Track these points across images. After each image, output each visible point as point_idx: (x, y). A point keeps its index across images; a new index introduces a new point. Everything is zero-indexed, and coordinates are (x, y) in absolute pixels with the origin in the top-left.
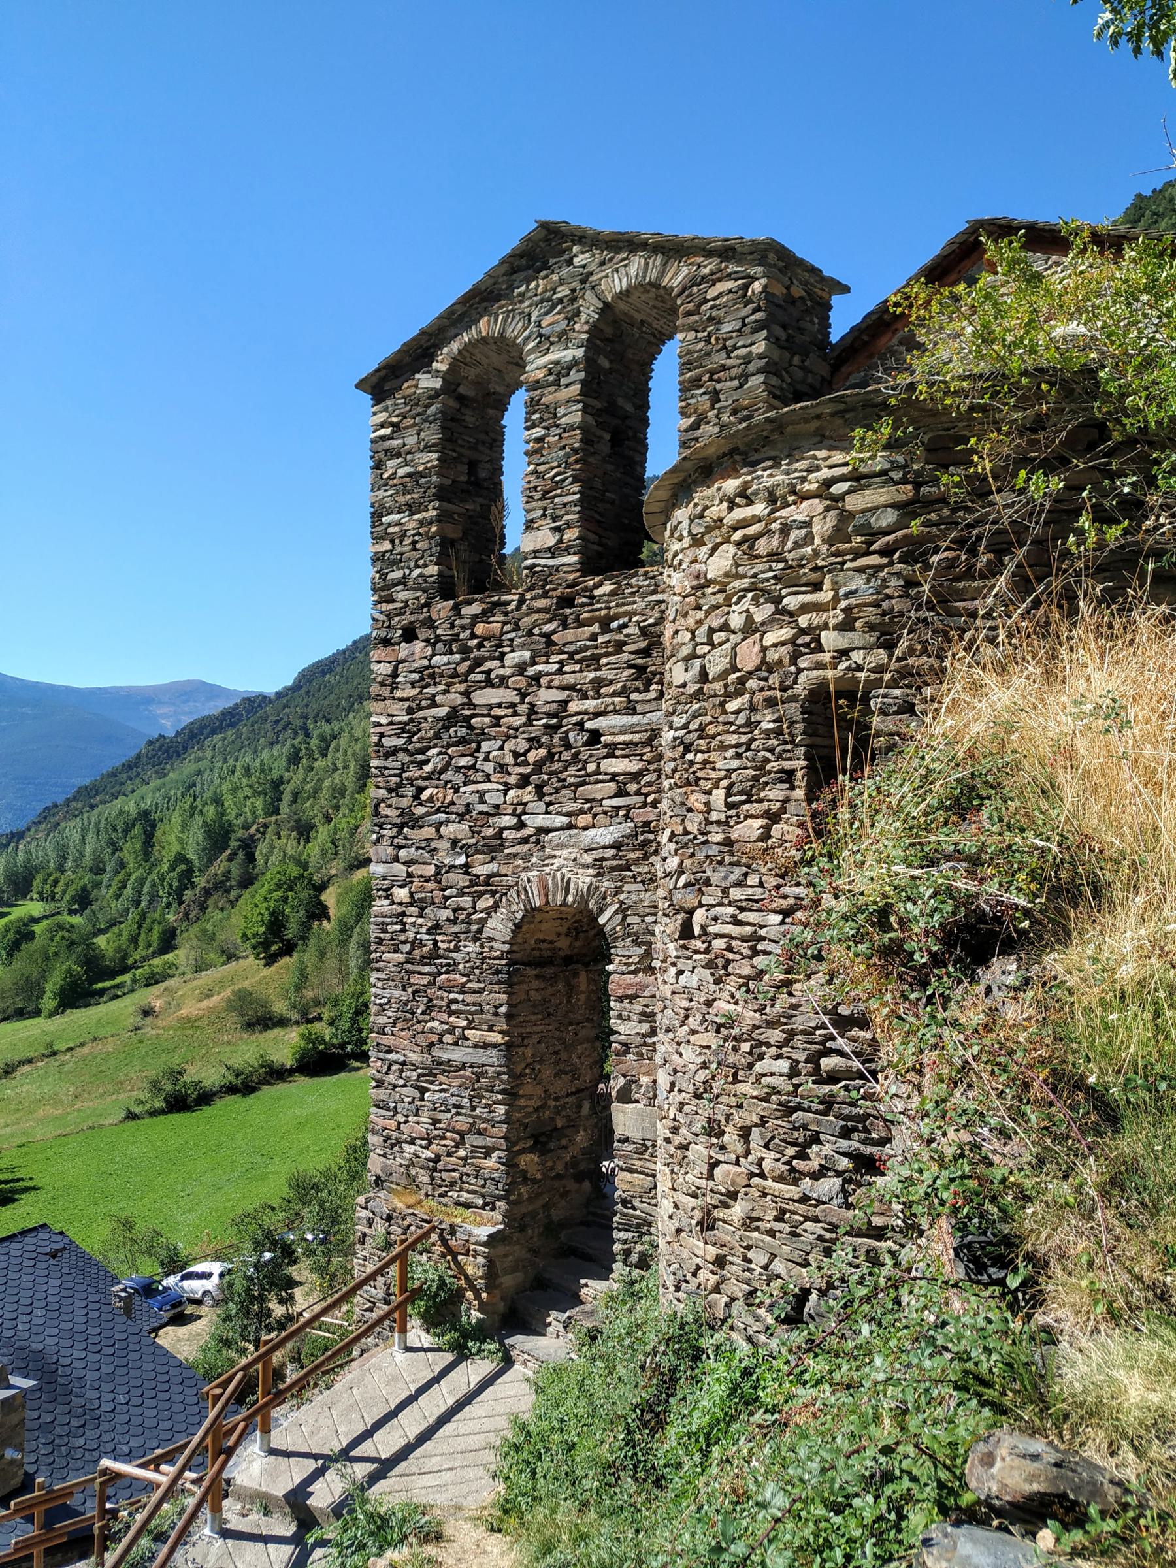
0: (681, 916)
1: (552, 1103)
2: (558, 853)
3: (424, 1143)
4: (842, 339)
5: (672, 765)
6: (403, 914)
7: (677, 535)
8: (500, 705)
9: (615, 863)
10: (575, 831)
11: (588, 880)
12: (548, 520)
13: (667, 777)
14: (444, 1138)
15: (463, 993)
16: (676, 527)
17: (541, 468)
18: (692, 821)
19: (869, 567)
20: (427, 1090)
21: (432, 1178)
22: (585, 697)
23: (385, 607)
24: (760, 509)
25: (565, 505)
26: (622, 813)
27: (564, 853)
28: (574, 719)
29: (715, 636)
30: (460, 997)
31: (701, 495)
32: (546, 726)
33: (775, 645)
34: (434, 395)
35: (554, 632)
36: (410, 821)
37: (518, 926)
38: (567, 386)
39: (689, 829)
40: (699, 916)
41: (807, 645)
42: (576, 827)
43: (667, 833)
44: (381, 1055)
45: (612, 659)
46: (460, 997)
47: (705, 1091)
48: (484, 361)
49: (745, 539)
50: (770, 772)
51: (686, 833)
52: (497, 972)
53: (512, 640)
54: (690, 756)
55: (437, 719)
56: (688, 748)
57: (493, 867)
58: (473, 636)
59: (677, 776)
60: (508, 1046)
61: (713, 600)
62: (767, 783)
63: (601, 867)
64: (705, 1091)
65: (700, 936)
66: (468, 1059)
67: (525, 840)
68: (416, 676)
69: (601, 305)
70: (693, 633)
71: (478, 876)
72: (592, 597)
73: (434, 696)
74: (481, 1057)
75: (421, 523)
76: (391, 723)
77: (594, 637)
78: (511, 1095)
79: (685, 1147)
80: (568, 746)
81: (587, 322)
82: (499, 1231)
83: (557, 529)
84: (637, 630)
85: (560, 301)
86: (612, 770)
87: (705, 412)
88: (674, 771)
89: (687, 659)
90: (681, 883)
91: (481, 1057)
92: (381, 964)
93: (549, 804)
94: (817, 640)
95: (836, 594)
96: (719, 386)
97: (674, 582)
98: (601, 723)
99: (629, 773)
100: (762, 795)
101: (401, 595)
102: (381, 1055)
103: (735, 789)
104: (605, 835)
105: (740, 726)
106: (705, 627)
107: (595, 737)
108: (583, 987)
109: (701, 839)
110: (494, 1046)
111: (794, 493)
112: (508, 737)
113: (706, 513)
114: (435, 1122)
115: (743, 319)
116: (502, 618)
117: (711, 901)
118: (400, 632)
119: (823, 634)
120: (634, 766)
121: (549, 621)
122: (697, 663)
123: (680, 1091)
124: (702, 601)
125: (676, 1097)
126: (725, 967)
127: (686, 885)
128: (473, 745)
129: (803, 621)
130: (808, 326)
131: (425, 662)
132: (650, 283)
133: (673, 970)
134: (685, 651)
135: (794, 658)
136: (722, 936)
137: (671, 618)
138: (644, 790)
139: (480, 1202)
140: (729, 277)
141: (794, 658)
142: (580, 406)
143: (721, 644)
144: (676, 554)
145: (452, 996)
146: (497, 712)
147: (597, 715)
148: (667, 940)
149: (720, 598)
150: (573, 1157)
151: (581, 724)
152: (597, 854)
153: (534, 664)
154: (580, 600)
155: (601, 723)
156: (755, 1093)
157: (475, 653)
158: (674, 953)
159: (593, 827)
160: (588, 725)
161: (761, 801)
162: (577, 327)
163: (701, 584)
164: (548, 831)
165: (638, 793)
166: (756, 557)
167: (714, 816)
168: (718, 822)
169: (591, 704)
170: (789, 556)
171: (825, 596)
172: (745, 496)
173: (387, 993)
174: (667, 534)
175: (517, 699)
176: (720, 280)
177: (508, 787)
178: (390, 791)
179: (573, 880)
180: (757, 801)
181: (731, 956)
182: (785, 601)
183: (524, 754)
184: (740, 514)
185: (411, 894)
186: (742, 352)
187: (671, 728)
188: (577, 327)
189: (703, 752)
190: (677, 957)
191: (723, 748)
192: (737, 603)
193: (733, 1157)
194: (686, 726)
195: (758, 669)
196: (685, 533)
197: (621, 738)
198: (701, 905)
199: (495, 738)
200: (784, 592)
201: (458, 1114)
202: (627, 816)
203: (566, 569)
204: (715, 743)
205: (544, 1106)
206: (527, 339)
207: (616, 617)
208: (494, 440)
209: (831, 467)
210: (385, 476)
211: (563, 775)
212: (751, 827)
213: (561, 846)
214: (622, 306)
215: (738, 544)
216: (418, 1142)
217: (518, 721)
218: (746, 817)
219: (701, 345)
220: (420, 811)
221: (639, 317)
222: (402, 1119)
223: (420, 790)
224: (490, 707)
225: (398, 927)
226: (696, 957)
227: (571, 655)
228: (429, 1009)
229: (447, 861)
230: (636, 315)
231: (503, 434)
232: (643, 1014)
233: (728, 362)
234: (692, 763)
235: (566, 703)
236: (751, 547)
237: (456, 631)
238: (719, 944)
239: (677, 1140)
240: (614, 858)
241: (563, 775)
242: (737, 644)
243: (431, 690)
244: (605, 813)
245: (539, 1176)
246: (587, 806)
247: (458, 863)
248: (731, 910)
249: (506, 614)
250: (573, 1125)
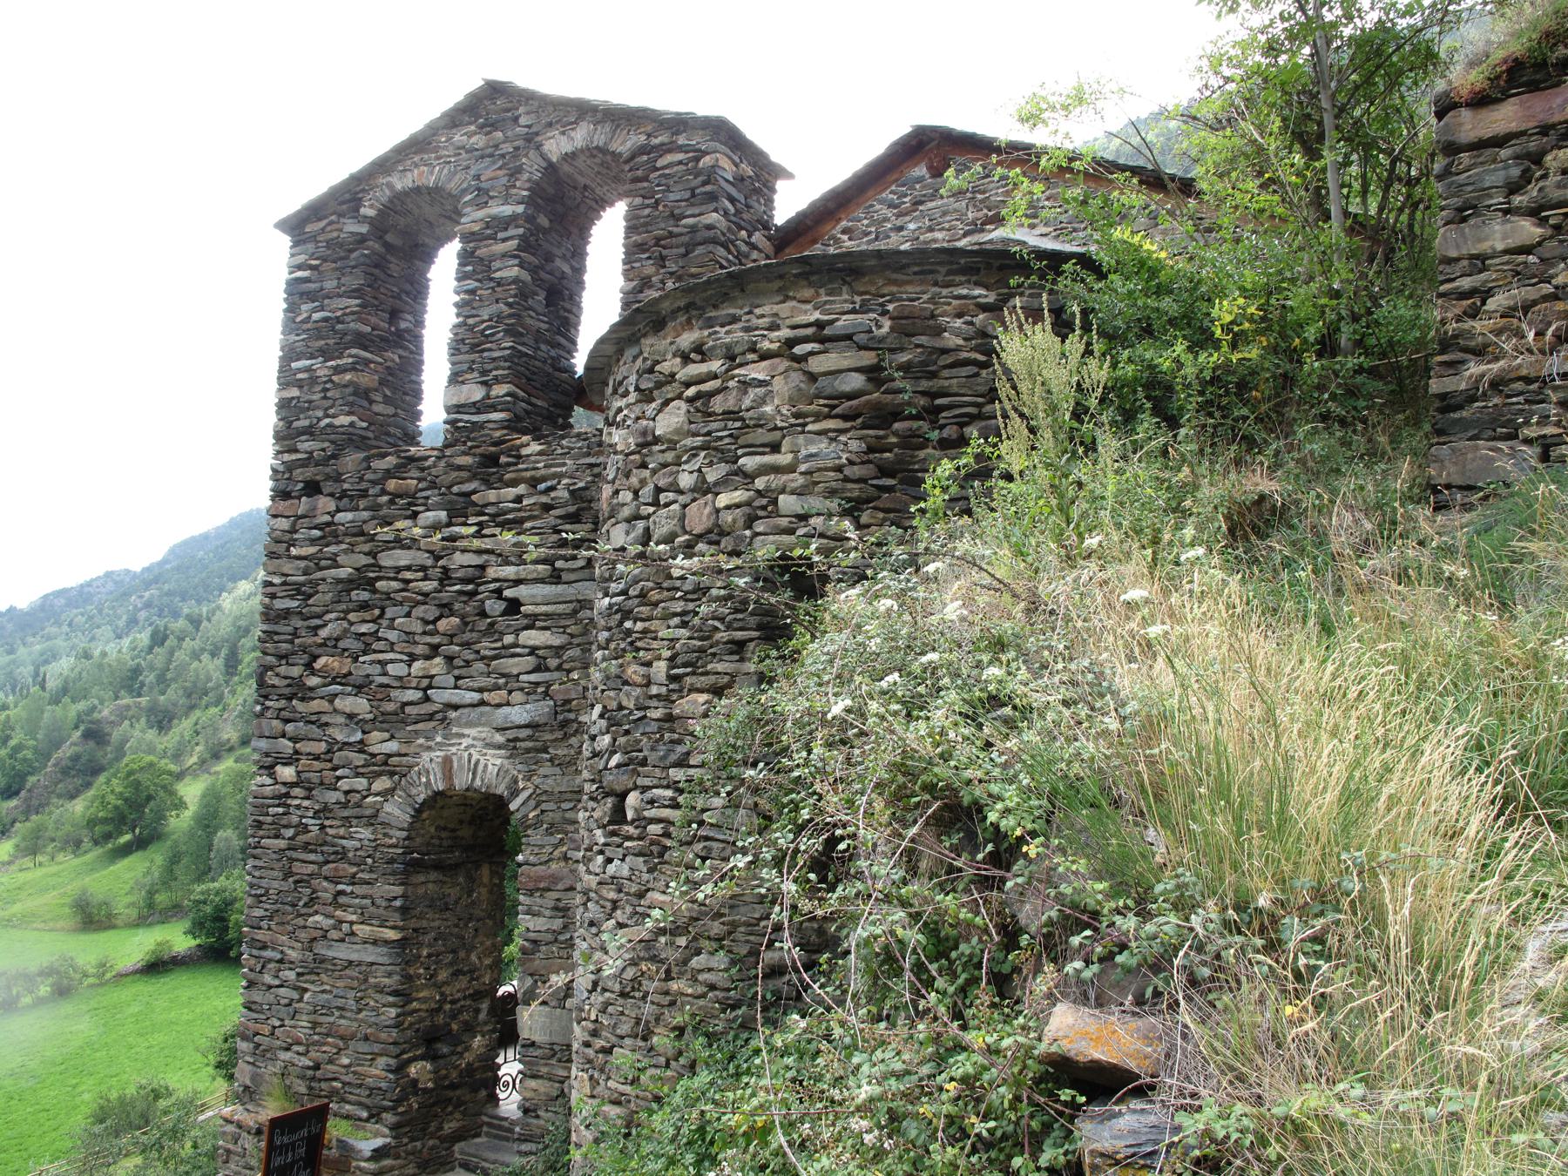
0: (610, 801)
1: (448, 1007)
2: (466, 731)
3: (301, 1049)
4: (788, 222)
5: (606, 634)
6: (287, 795)
7: (621, 390)
8: (408, 568)
9: (530, 744)
10: (488, 708)
11: (498, 762)
12: (476, 374)
13: (600, 648)
14: (325, 1044)
15: (353, 884)
16: (621, 383)
17: (471, 321)
18: (628, 695)
19: (830, 430)
20: (306, 990)
21: (310, 1088)
22: (508, 563)
23: (287, 457)
24: (716, 365)
25: (494, 359)
26: (540, 690)
27: (473, 732)
28: (492, 586)
29: (662, 496)
30: (349, 889)
31: (650, 344)
32: (460, 593)
33: (728, 507)
34: (361, 240)
35: (474, 492)
36: (299, 691)
37: (419, 811)
38: (504, 240)
39: (625, 703)
40: (632, 799)
41: (764, 508)
42: (488, 704)
43: (598, 709)
44: (255, 952)
45: (537, 523)
46: (349, 889)
47: (633, 989)
48: (416, 211)
49: (699, 395)
50: (718, 643)
51: (621, 708)
52: (391, 861)
53: (427, 498)
54: (628, 624)
55: (339, 581)
56: (627, 614)
57: (392, 746)
58: (384, 492)
59: (612, 646)
60: (402, 943)
61: (661, 458)
62: (714, 655)
63: (515, 748)
64: (633, 989)
65: (633, 821)
66: (354, 957)
67: (430, 717)
68: (317, 533)
69: (544, 165)
70: (636, 493)
71: (373, 755)
72: (519, 457)
73: (336, 555)
74: (370, 955)
75: (338, 370)
76: (284, 583)
77: (518, 499)
78: (402, 995)
79: (608, 1051)
80: (483, 614)
81: (529, 180)
82: (385, 1146)
83: (484, 383)
84: (566, 494)
85: (503, 156)
86: (531, 643)
87: (650, 277)
88: (608, 641)
89: (628, 521)
90: (612, 763)
91: (370, 955)
92: (259, 851)
93: (458, 678)
94: (775, 502)
95: (796, 458)
96: (665, 252)
97: (616, 439)
98: (521, 592)
99: (550, 647)
100: (709, 667)
101: (306, 445)
102: (255, 952)
103: (679, 660)
104: (519, 714)
105: (686, 593)
106: (650, 487)
107: (514, 606)
108: (486, 880)
109: (639, 714)
110: (386, 942)
111: (754, 350)
112: (418, 603)
113: (657, 368)
114: (315, 1025)
115: (693, 190)
116: (417, 474)
117: (647, 782)
118: (300, 485)
119: (781, 497)
120: (557, 640)
121: (469, 480)
122: (641, 524)
123: (604, 990)
124: (648, 459)
125: (597, 999)
126: (661, 855)
127: (618, 766)
128: (377, 612)
129: (760, 483)
130: (756, 205)
131: (327, 518)
132: (597, 147)
133: (600, 859)
134: (626, 512)
135: (750, 521)
136: (660, 821)
137: (610, 477)
138: (566, 666)
139: (365, 1114)
140: (681, 149)
141: (750, 521)
142: (516, 261)
143: (667, 505)
144: (620, 410)
145: (340, 887)
146: (408, 575)
147: (518, 582)
148: (594, 825)
149: (669, 457)
150: (468, 1064)
151: (498, 593)
152: (511, 734)
153: (449, 525)
154: (503, 459)
155: (521, 592)
156: (690, 991)
157: (385, 511)
158: (602, 840)
159: (508, 704)
160: (507, 593)
161: (706, 673)
162: (518, 184)
163: (648, 441)
164: (456, 707)
165: (559, 668)
166: (710, 415)
167: (654, 690)
168: (658, 696)
169: (509, 571)
170: (747, 415)
171: (784, 458)
172: (700, 352)
173: (264, 883)
174: (610, 390)
175: (429, 562)
176: (670, 151)
177: (413, 658)
178: (280, 657)
179: (482, 762)
180: (703, 674)
181: (669, 843)
182: (741, 461)
183: (434, 622)
184: (695, 369)
185: (298, 773)
186: (690, 221)
187: (606, 595)
188: (518, 184)
189: (643, 620)
190: (605, 845)
191: (666, 617)
192: (686, 462)
193: (662, 1060)
194: (624, 592)
195: (709, 531)
196: (632, 389)
197: (543, 609)
198: (636, 787)
199: (401, 604)
200: (740, 452)
201: (341, 1017)
202: (546, 694)
203: (491, 426)
204: (658, 611)
205: (438, 1010)
206: (464, 191)
207: (544, 479)
208: (416, 290)
209: (794, 327)
210: (299, 319)
211: (477, 647)
212: (695, 701)
213: (470, 724)
214: (566, 168)
215: (690, 400)
216: (295, 1048)
217: (428, 586)
218: (690, 691)
219: (647, 211)
220: (313, 681)
221: (582, 181)
222: (277, 1023)
223: (315, 658)
224: (399, 570)
225: (281, 810)
226: (627, 844)
227: (493, 516)
228: (312, 901)
229: (339, 737)
230: (579, 178)
231: (427, 287)
232: (556, 908)
233: (676, 230)
234: (629, 632)
235: (483, 568)
236: (706, 404)
237: (364, 485)
238: (655, 829)
239: (599, 1043)
240: (530, 738)
241: (477, 647)
242: (685, 506)
243: (332, 549)
244: (522, 689)
245: (430, 1085)
246: (502, 681)
247: (352, 739)
248: (669, 793)
249: (422, 470)
250: (470, 1029)
